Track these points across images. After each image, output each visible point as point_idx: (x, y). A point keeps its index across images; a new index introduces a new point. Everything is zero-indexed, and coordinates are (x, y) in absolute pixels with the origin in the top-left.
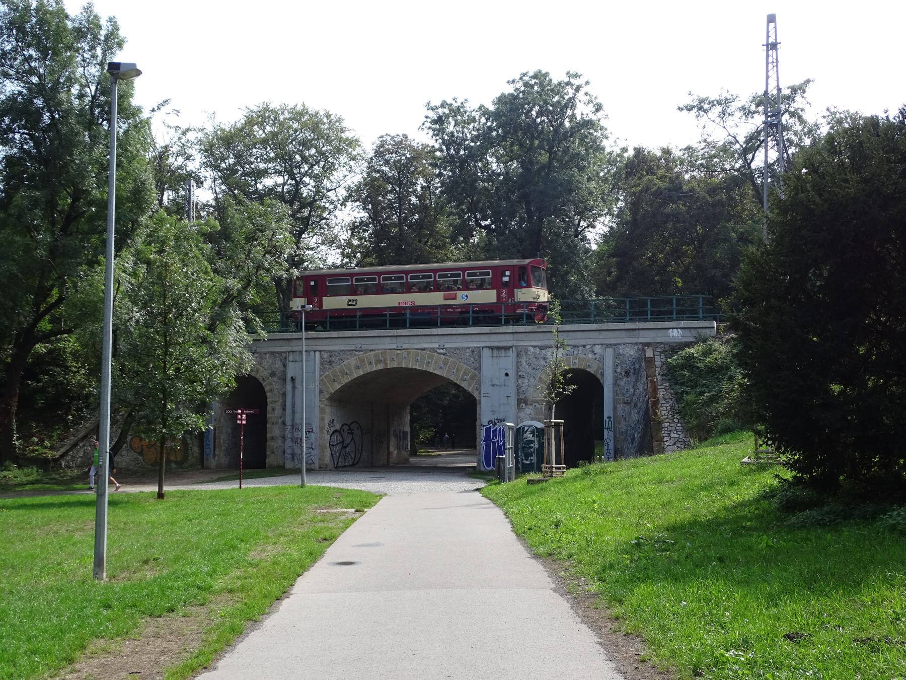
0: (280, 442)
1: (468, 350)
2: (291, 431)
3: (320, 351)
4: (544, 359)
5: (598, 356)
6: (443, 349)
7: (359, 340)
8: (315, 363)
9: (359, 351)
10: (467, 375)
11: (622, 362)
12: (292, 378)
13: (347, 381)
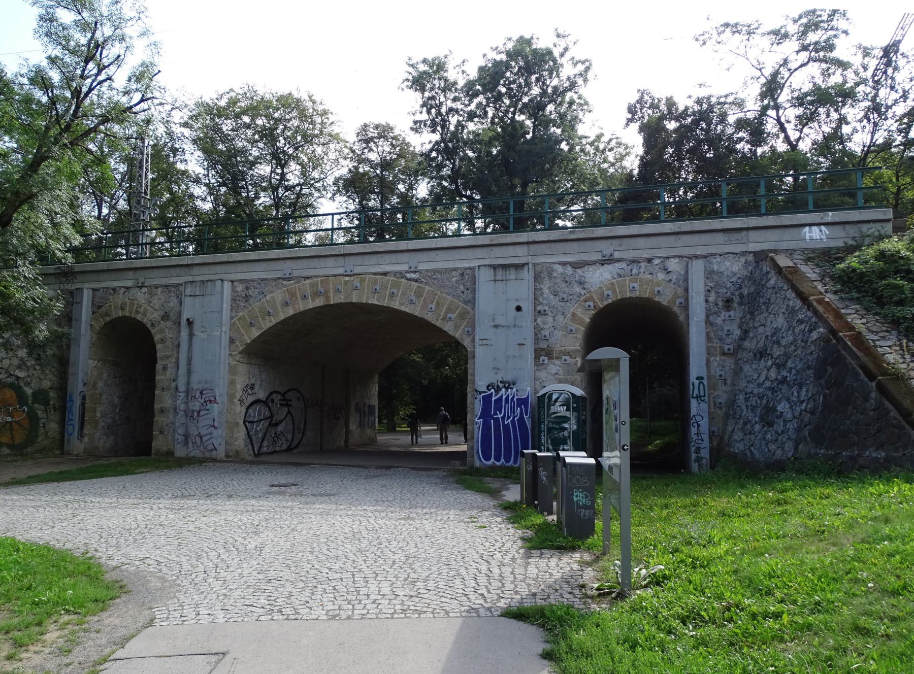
0: (171, 416)
1: (454, 273)
2: (185, 400)
3: (232, 281)
4: (581, 283)
5: (674, 277)
6: (415, 272)
7: (289, 263)
8: (222, 297)
9: (288, 279)
10: (453, 313)
11: (717, 285)
12: (188, 320)
13: (269, 325)
